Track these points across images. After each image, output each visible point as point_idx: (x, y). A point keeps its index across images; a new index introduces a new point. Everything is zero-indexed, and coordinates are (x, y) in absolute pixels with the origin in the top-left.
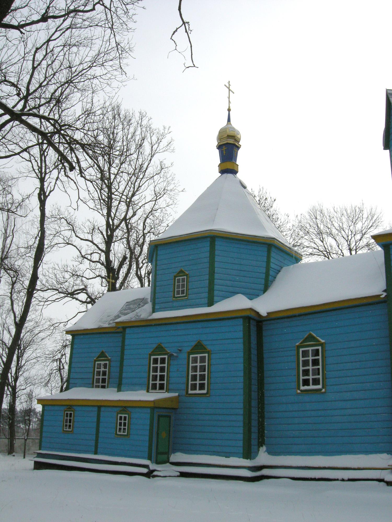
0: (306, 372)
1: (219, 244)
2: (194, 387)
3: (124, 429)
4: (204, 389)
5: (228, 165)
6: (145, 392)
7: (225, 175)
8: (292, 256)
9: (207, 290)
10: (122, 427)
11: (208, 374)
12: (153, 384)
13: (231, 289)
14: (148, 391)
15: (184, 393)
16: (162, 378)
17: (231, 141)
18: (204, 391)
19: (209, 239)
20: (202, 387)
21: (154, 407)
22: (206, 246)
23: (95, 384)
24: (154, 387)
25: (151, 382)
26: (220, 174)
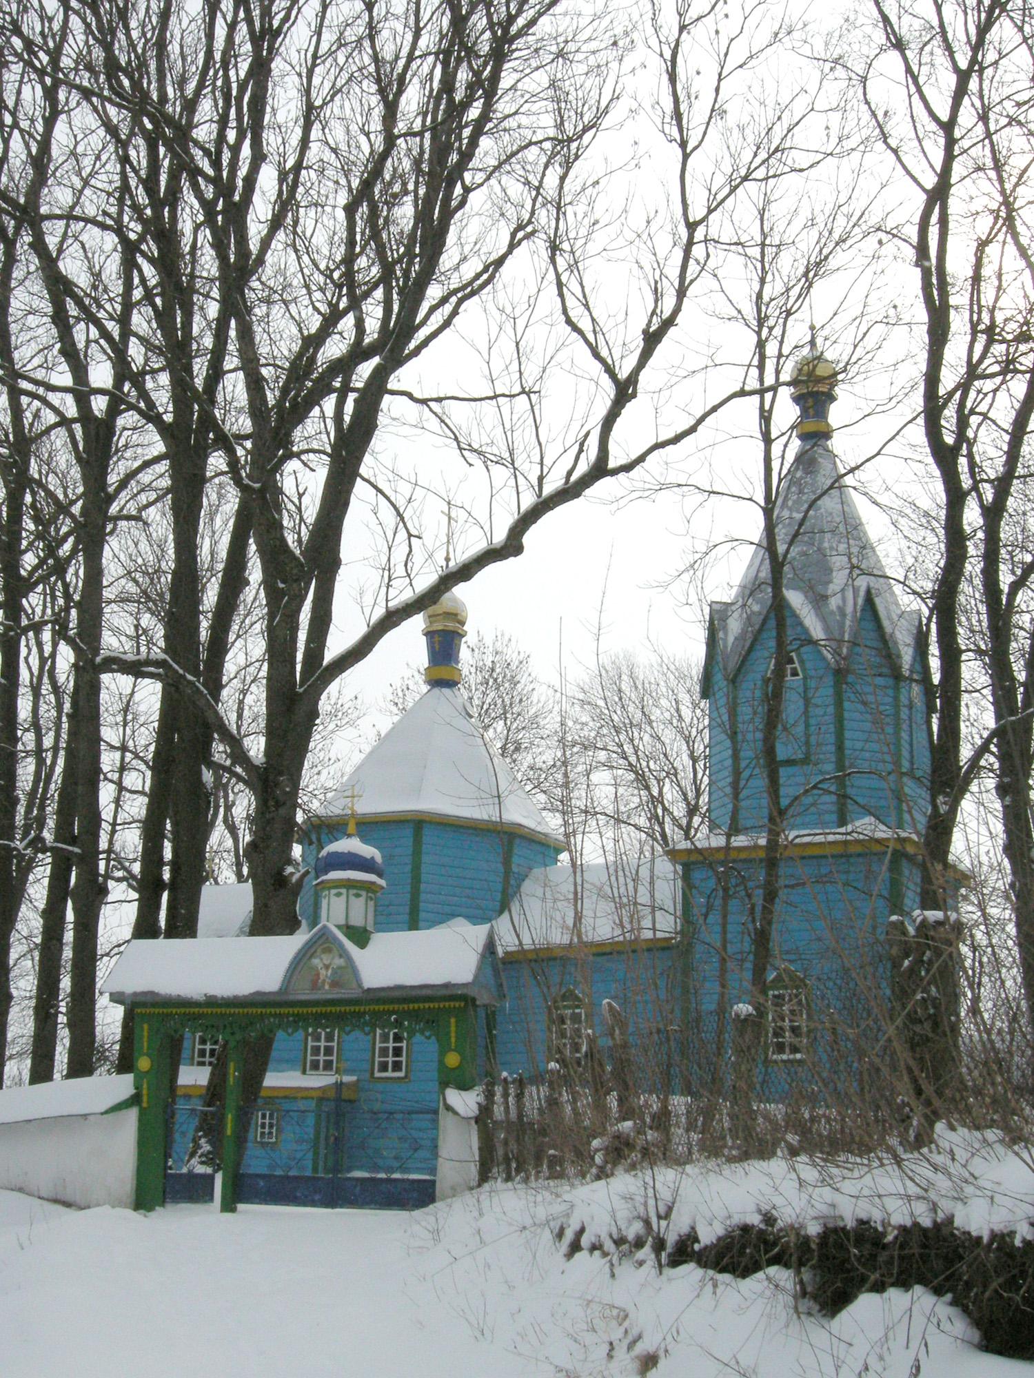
0: (316, 1050)
1: (428, 836)
2: (384, 1067)
3: (270, 1133)
4: (400, 1070)
5: (443, 673)
6: (298, 1073)
7: (436, 691)
8: (548, 846)
9: (407, 909)
10: (267, 1130)
11: (374, 1044)
12: (312, 1061)
13: (447, 909)
14: (304, 1072)
15: (368, 1075)
16: (328, 1051)
17: (451, 625)
18: (401, 1074)
19: (412, 825)
20: (397, 1066)
21: (321, 1096)
22: (408, 832)
23: (197, 1059)
24: (315, 1066)
25: (309, 1058)
26: (425, 688)
